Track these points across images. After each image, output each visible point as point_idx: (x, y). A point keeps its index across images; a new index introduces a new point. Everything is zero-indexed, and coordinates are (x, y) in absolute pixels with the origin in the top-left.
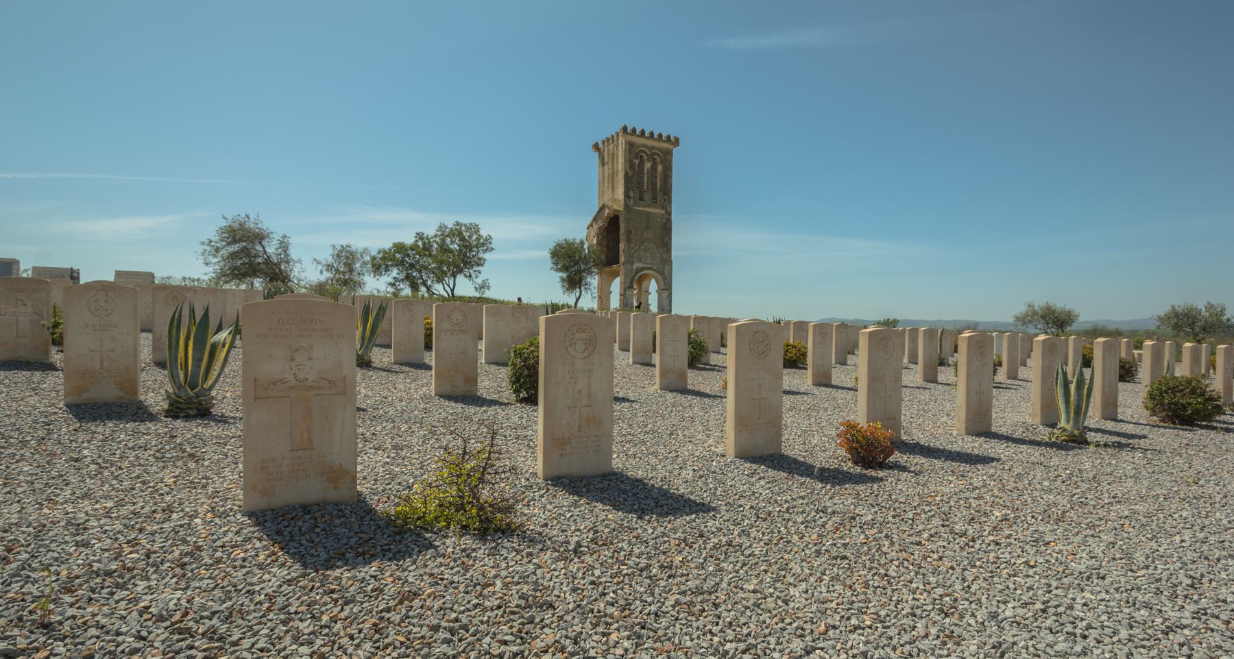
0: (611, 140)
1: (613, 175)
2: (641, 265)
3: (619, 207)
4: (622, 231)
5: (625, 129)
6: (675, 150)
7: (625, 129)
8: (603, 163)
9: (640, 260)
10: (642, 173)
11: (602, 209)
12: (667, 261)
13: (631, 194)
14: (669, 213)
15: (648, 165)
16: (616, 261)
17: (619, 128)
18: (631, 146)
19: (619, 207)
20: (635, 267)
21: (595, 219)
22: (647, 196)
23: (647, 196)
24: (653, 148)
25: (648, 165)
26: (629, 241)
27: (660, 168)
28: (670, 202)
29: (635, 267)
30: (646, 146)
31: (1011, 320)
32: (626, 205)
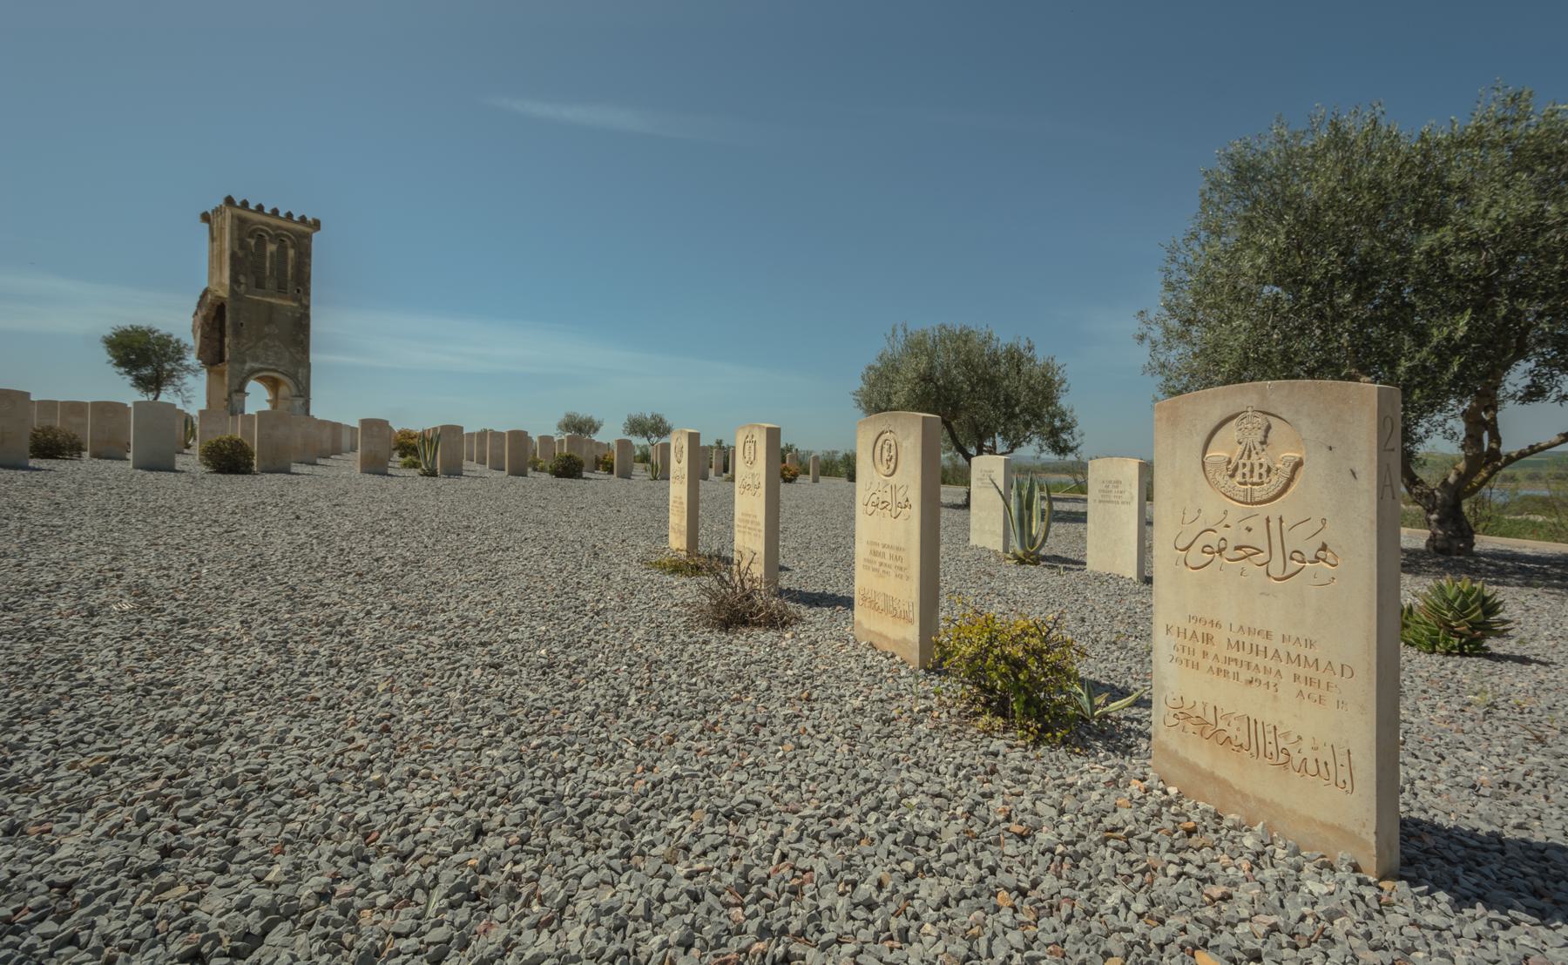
0: (217, 211)
1: (221, 252)
2: (257, 365)
3: (224, 293)
4: (228, 323)
5: (229, 201)
6: (315, 236)
7: (229, 201)
8: (212, 239)
9: (256, 359)
10: (263, 256)
11: (206, 292)
12: (1286, 366)
13: (242, 279)
14: (308, 307)
15: (271, 248)
16: (222, 360)
17: (220, 202)
18: (241, 222)
19: (224, 293)
20: (247, 366)
21: (200, 305)
22: (270, 284)
23: (270, 284)
24: (279, 228)
25: (271, 248)
26: (237, 333)
27: (291, 253)
28: (308, 294)
29: (247, 366)
30: (268, 225)
31: (396, 429)
32: (233, 292)
